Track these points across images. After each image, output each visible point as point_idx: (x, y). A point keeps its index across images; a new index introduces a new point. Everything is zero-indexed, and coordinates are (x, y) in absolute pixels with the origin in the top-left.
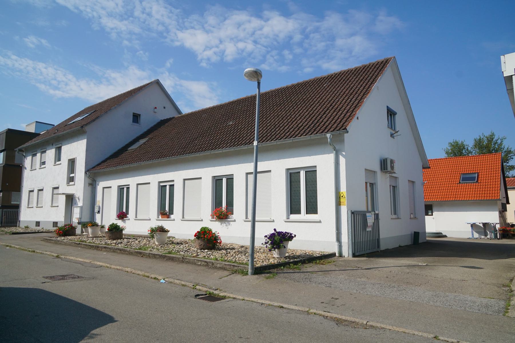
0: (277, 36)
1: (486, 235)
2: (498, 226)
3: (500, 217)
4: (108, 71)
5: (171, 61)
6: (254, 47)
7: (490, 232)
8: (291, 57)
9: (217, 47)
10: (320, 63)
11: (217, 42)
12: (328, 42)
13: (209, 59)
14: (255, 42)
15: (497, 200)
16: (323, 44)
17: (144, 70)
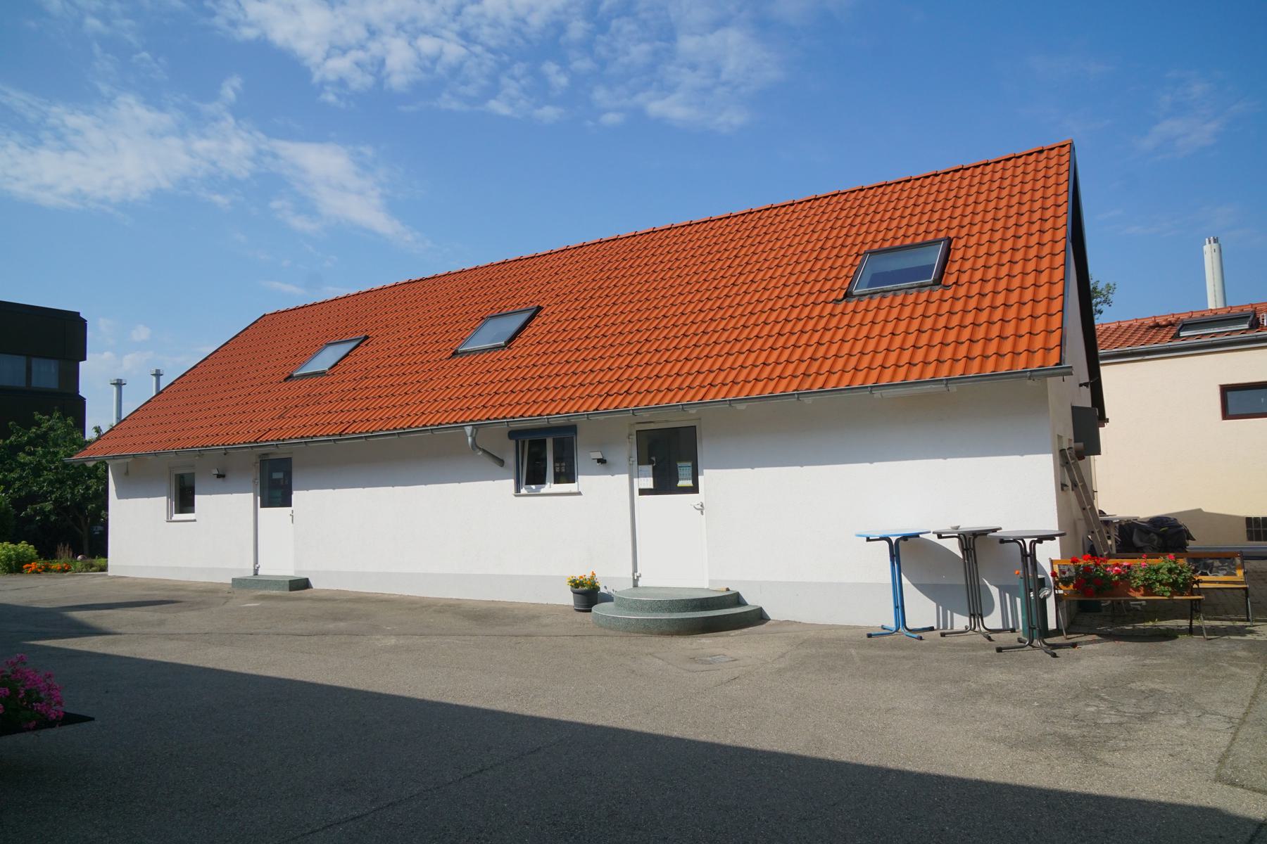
0: (524, 21)
1: (977, 611)
2: (1048, 554)
3: (1062, 487)
4: (55, 109)
5: (236, 81)
6: (463, 51)
7: (1003, 590)
8: (563, 80)
9: (362, 47)
10: (640, 98)
11: (362, 33)
12: (658, 44)
13: (342, 83)
14: (466, 36)
15: (1043, 373)
16: (645, 47)
17: (161, 109)
